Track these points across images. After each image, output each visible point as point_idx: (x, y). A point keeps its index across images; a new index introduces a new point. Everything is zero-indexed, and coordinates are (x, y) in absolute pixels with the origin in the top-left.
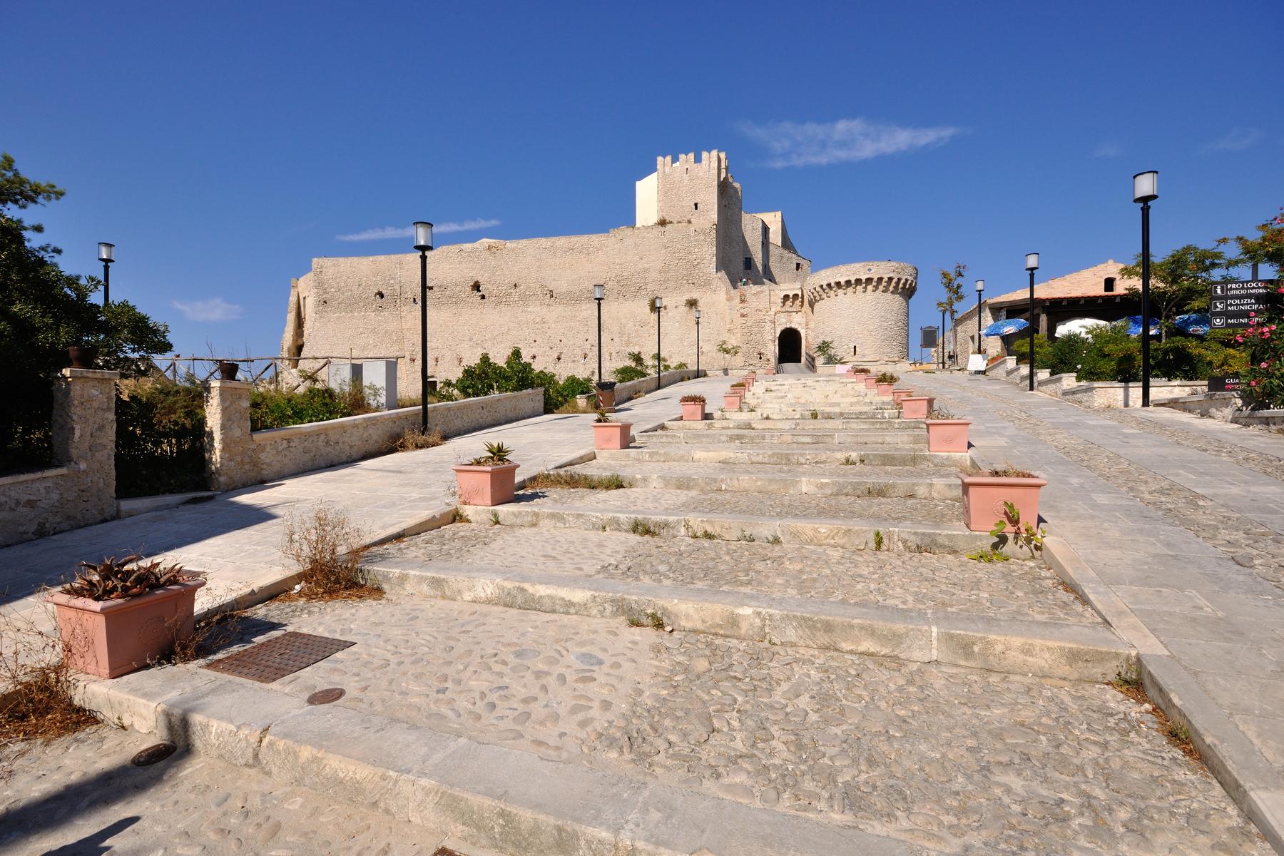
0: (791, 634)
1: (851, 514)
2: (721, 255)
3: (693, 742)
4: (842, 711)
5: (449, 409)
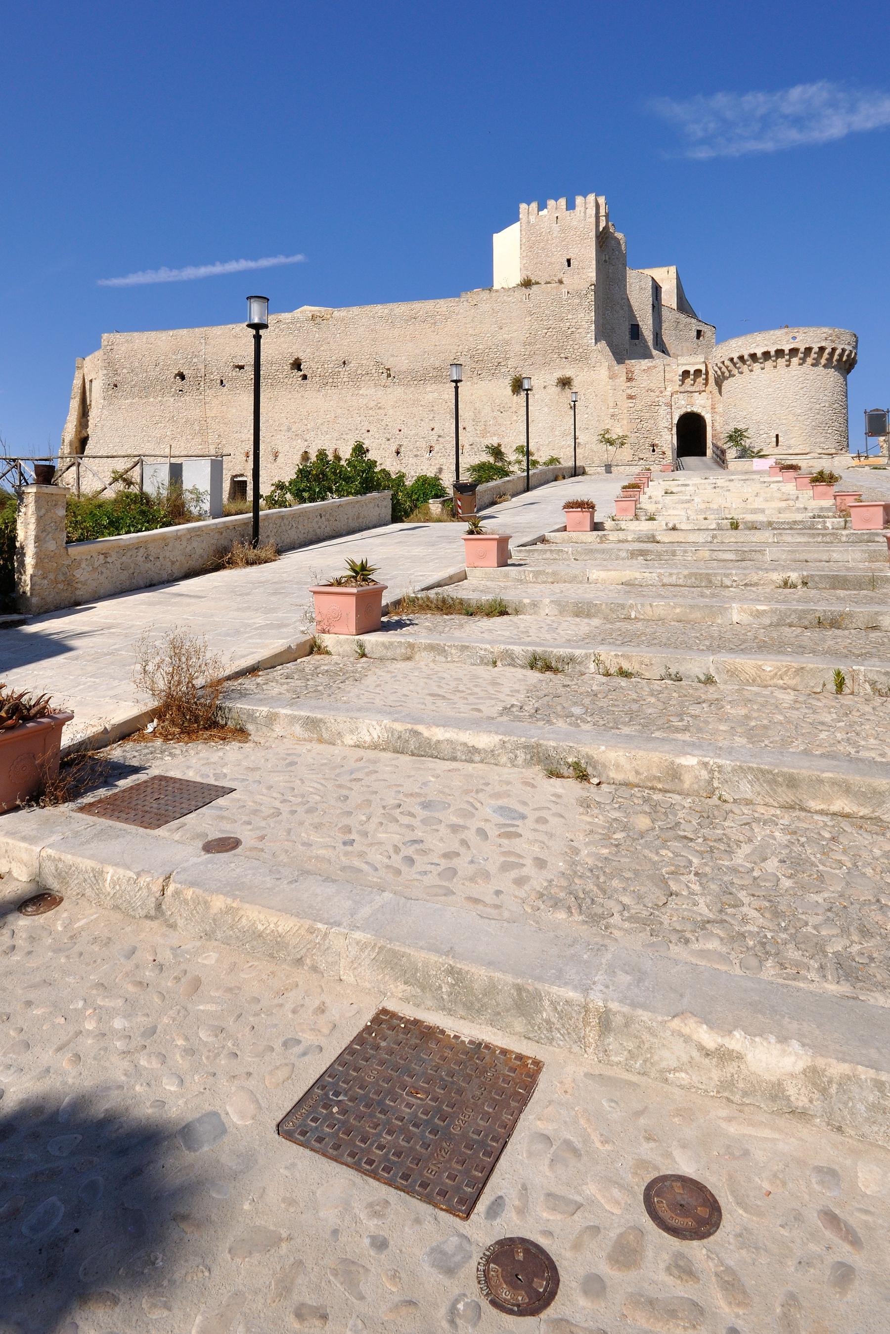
0: (746, 789)
1: (801, 650)
2: (601, 321)
3: (650, 905)
4: (821, 876)
5: (282, 517)
